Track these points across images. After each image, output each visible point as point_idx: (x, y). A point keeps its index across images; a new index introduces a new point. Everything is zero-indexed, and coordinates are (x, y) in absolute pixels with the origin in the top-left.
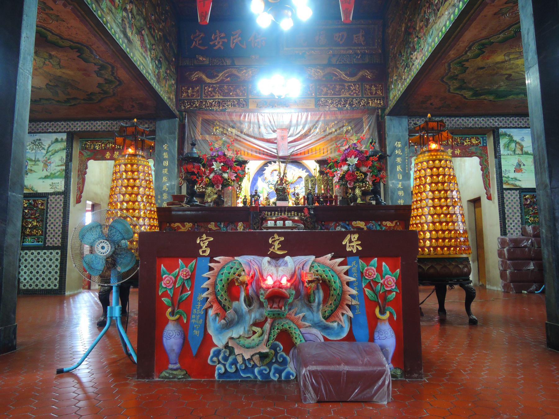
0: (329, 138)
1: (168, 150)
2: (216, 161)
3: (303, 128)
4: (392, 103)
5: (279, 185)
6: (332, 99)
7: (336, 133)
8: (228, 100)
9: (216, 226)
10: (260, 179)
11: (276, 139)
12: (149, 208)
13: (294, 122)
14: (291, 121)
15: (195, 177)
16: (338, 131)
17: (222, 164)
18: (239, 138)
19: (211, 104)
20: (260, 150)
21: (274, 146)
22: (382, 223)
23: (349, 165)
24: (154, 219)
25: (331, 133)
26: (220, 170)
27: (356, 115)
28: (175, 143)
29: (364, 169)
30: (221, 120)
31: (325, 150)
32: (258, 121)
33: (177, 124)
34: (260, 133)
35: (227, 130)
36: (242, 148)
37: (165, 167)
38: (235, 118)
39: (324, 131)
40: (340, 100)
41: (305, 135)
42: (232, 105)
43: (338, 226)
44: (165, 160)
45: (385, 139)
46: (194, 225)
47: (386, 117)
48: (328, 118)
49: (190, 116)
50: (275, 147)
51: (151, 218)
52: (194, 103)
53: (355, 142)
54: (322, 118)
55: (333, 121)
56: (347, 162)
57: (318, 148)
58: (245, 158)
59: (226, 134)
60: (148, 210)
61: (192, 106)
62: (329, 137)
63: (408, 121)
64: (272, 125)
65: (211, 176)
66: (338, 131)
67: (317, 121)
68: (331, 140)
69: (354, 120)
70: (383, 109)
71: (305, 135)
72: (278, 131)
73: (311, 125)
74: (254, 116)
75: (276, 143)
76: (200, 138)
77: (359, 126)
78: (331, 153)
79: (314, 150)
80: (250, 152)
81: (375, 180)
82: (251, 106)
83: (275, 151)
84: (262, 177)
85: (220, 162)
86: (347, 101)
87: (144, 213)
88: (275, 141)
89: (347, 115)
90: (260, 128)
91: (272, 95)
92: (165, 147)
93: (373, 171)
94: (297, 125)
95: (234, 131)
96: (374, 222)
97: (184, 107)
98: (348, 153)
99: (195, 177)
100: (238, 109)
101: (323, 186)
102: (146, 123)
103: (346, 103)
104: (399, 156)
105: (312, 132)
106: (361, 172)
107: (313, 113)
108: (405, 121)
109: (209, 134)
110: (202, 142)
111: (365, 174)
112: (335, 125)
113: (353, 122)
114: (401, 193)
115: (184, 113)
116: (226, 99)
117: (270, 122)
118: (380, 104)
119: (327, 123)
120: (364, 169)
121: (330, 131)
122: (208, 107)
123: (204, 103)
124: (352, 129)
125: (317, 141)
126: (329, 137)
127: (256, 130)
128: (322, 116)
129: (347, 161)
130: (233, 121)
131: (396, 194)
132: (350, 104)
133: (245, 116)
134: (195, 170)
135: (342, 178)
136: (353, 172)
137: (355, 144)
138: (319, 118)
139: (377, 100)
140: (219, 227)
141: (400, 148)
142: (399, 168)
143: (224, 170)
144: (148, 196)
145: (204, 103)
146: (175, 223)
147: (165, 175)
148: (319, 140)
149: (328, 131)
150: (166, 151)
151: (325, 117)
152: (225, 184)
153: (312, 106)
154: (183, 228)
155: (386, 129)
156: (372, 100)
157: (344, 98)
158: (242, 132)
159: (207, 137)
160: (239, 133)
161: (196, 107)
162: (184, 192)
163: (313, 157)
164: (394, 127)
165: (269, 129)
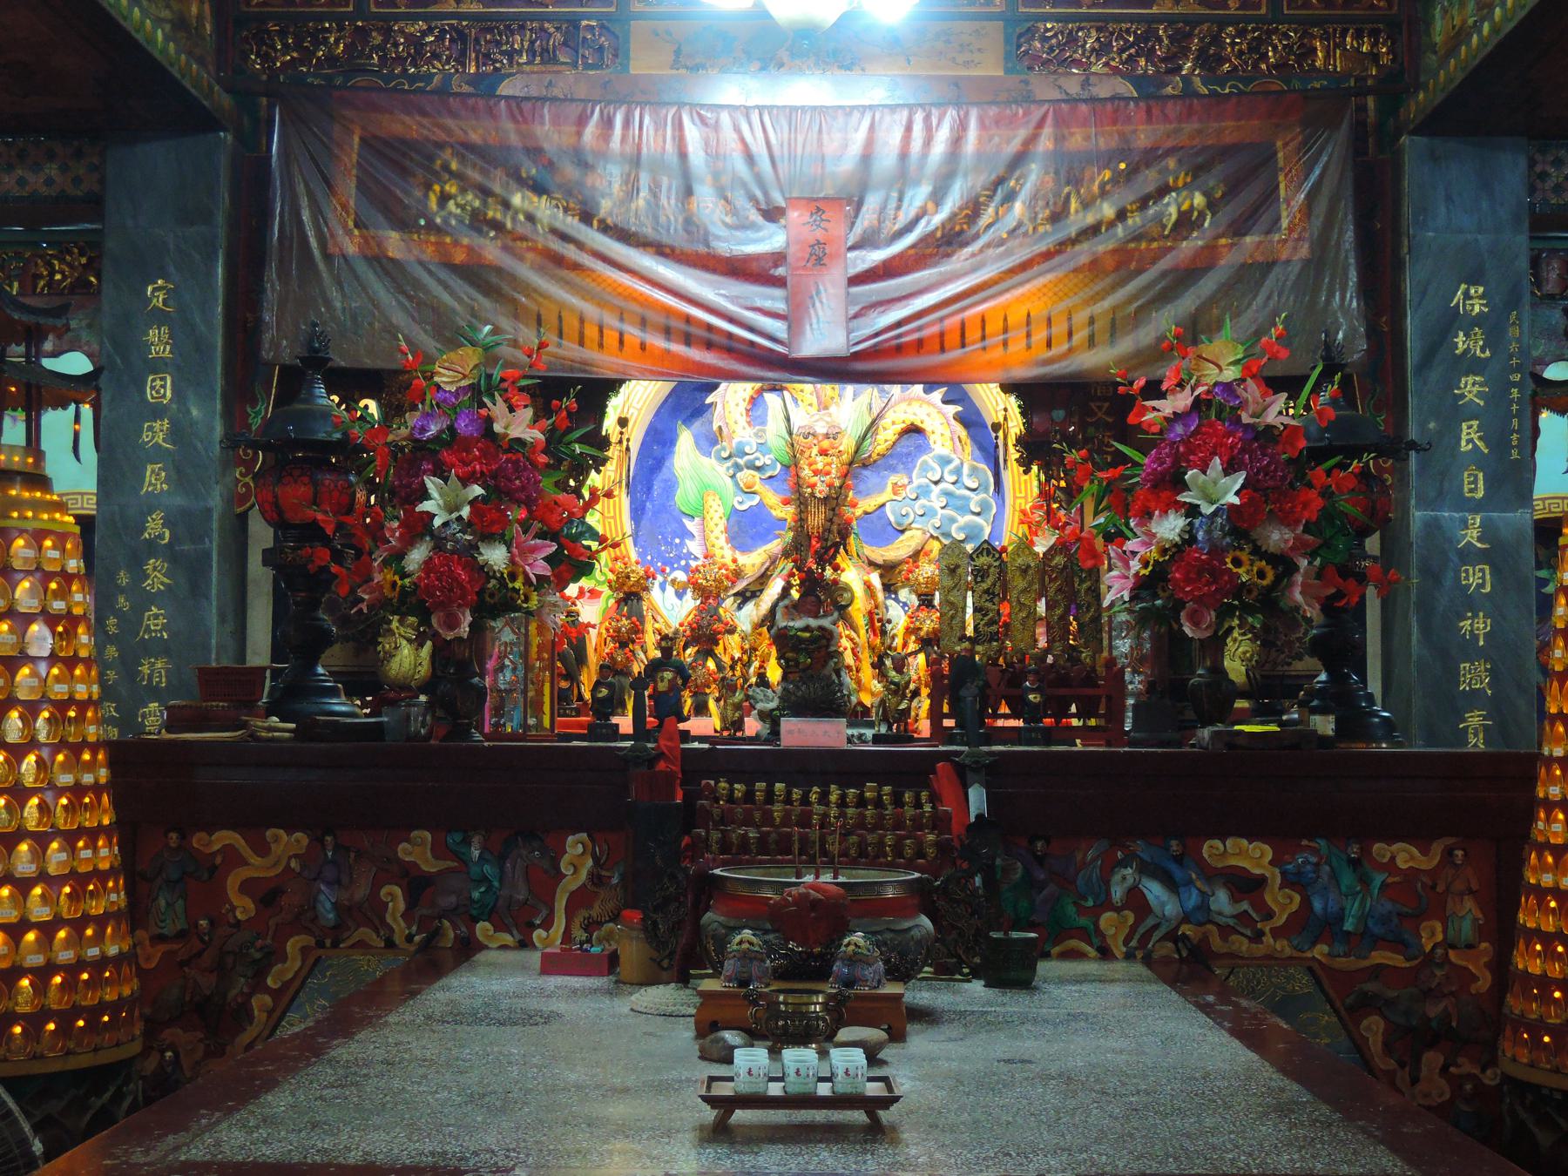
0: (1084, 259)
1: (172, 312)
2: (441, 472)
3: (937, 197)
4: (1444, 75)
5: (796, 609)
6: (1101, 23)
7: (1120, 230)
8: (517, 24)
9: (439, 851)
10: (685, 439)
11: (779, 258)
12: (66, 779)
13: (887, 159)
14: (866, 158)
15: (322, 556)
16: (1134, 220)
17: (477, 490)
18: (570, 252)
19: (416, 42)
20: (688, 319)
21: (773, 299)
22: (1365, 851)
23: (1192, 511)
24: (92, 835)
25: (1093, 230)
26: (467, 526)
27: (1230, 130)
28: (210, 273)
29: (1277, 537)
30: (469, 147)
31: (1059, 329)
32: (683, 155)
33: (223, 161)
34: (689, 222)
35: (506, 205)
36: (590, 309)
37: (157, 412)
38: (549, 133)
39: (1056, 217)
40: (1150, 35)
41: (947, 241)
42: (532, 52)
43: (1123, 864)
44: (156, 367)
45: (1399, 266)
46: (318, 841)
47: (1404, 139)
48: (1077, 140)
49: (294, 120)
50: (780, 306)
51: (81, 832)
52: (319, 38)
53: (1231, 374)
54: (1045, 143)
55: (1108, 160)
56: (1184, 498)
57: (1017, 316)
58: (604, 363)
59: (498, 226)
60: (61, 791)
61: (307, 55)
62: (1083, 253)
63: (1532, 163)
64: (759, 179)
65: (417, 556)
66: (1134, 220)
67: (1019, 160)
68: (1094, 266)
69: (1225, 152)
70: (1395, 86)
71: (947, 241)
72: (793, 215)
73: (981, 180)
74: (659, 126)
75: (780, 282)
76: (351, 249)
77: (1248, 196)
78: (1091, 342)
79: (994, 326)
80: (633, 333)
81: (1339, 595)
82: (640, 65)
83: (777, 327)
84: (697, 424)
85: (465, 481)
86: (1190, 35)
87: (43, 807)
88: (780, 271)
89: (1191, 126)
90: (688, 192)
91: (762, 15)
92: (156, 294)
93: (1327, 544)
94: (903, 177)
95: (544, 209)
96: (1322, 843)
97: (265, 58)
98: (1185, 441)
99: (322, 556)
100: (568, 81)
101: (1041, 608)
102: (51, 156)
103: (1184, 52)
104: (1475, 366)
105: (985, 220)
106: (1257, 552)
107: (993, 111)
108: (1511, 170)
109: (404, 224)
110: (362, 267)
111: (1283, 564)
112: (1115, 180)
113: (1219, 169)
114: (1477, 578)
115: (264, 101)
116: (500, 17)
117: (750, 158)
118: (1374, 57)
119: (1070, 172)
120: (1277, 537)
121: (1090, 219)
122: (400, 60)
123: (377, 39)
124: (1212, 205)
125: (1012, 271)
126: (1083, 253)
127: (669, 204)
128: (1047, 131)
129: (1184, 487)
130: (535, 152)
131: (1448, 582)
132: (1203, 60)
133: (608, 123)
134: (324, 517)
135: (1143, 587)
136: (1217, 552)
137: (1228, 387)
138: (1032, 140)
139: (1358, 36)
140: (457, 856)
141: (1479, 321)
142: (1469, 436)
143: (486, 525)
144: (61, 706)
145: (377, 39)
146: (210, 829)
147: (157, 454)
148: (1024, 266)
149: (1078, 219)
150: (159, 317)
151: (1059, 139)
152: (496, 600)
153: (991, 67)
154: (255, 860)
155: (1407, 210)
156: (1325, 37)
157: (1169, 20)
158: (587, 217)
159: (394, 243)
160: (571, 224)
161: (331, 59)
162: (259, 651)
163: (990, 365)
164: (1449, 198)
165: (741, 201)
